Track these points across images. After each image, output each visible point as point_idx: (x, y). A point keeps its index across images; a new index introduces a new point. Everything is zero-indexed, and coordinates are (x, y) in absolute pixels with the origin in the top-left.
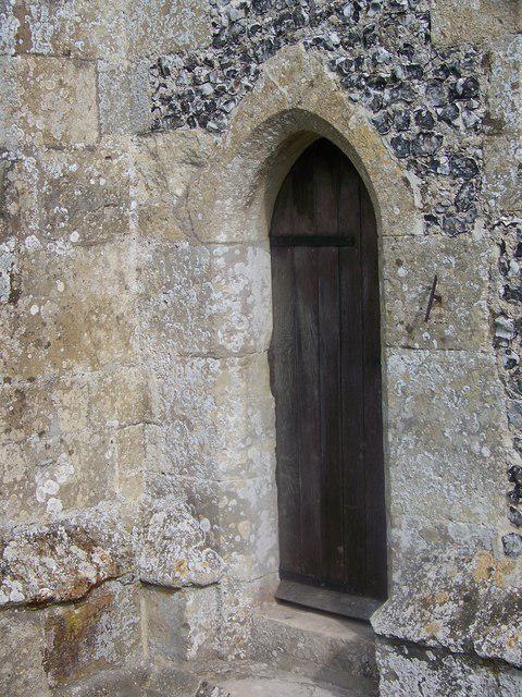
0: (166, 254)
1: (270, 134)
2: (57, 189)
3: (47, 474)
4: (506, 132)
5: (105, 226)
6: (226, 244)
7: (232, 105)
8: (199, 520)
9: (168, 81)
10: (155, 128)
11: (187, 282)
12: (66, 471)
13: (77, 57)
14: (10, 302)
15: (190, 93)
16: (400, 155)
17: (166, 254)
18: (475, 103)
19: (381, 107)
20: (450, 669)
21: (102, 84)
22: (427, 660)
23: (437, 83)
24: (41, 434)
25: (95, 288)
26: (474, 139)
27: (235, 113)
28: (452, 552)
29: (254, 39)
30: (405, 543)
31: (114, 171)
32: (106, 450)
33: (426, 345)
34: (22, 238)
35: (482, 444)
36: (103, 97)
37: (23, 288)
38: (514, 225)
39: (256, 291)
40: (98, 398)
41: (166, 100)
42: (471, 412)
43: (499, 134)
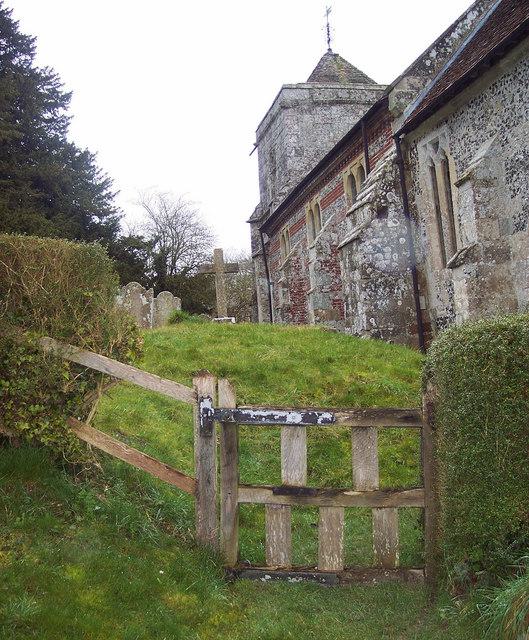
2: (487, 251)
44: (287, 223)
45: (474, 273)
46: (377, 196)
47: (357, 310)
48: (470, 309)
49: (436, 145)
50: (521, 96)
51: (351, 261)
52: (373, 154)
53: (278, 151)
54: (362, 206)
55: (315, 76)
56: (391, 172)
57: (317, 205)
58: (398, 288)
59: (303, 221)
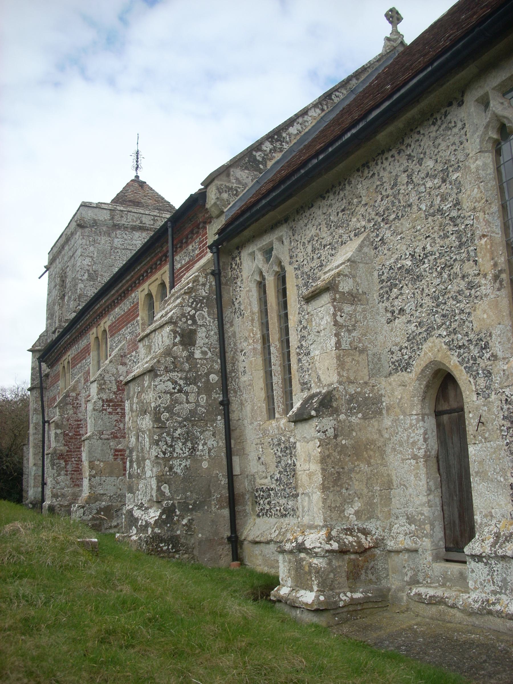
0: (395, 421)
1: (428, 371)
2: (352, 398)
3: (350, 506)
4: (499, 359)
5: (372, 411)
6: (416, 415)
7: (414, 362)
8: (411, 526)
9: (394, 356)
10: (390, 374)
11: (403, 431)
12: (357, 505)
13: (359, 350)
14: (334, 438)
15: (401, 359)
16: (467, 372)
17: (395, 421)
18: (488, 350)
19: (461, 356)
20: (491, 564)
21: (370, 359)
22: (483, 562)
23: (477, 345)
24: (347, 489)
25: (368, 435)
26: (489, 363)
27: (415, 365)
28: (494, 521)
29: (420, 337)
30: (479, 521)
31: (375, 391)
32: (374, 499)
33: (481, 442)
34: (338, 415)
35: (500, 477)
36: (370, 364)
37: (339, 433)
38: (504, 392)
39: (429, 432)
40: (371, 478)
41: (393, 363)
42: (496, 465)
43: (496, 360)
44: (69, 353)
45: (331, 432)
46: (183, 315)
47: (144, 472)
48: (324, 488)
49: (268, 252)
50: (410, 176)
51: (140, 402)
52: (179, 266)
53: (69, 273)
54: (162, 327)
55: (120, 199)
56: (204, 285)
57: (105, 331)
58: (205, 444)
59: (86, 351)
